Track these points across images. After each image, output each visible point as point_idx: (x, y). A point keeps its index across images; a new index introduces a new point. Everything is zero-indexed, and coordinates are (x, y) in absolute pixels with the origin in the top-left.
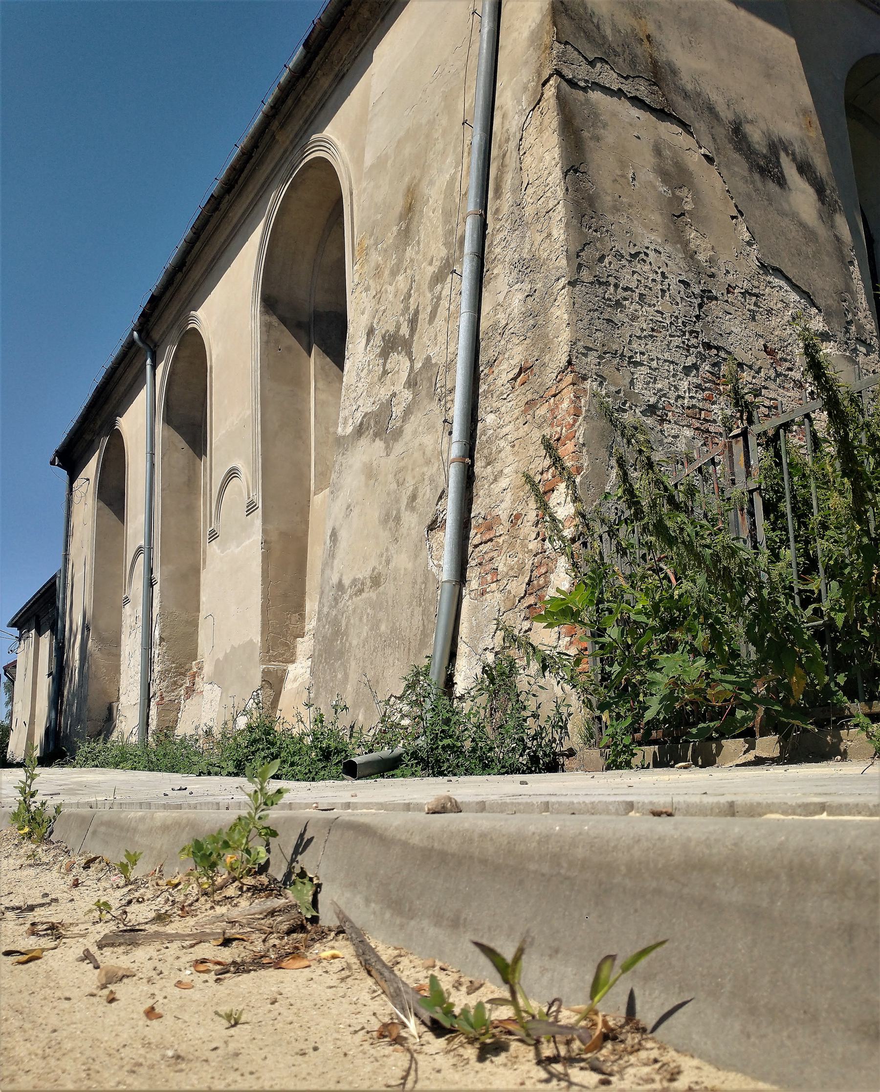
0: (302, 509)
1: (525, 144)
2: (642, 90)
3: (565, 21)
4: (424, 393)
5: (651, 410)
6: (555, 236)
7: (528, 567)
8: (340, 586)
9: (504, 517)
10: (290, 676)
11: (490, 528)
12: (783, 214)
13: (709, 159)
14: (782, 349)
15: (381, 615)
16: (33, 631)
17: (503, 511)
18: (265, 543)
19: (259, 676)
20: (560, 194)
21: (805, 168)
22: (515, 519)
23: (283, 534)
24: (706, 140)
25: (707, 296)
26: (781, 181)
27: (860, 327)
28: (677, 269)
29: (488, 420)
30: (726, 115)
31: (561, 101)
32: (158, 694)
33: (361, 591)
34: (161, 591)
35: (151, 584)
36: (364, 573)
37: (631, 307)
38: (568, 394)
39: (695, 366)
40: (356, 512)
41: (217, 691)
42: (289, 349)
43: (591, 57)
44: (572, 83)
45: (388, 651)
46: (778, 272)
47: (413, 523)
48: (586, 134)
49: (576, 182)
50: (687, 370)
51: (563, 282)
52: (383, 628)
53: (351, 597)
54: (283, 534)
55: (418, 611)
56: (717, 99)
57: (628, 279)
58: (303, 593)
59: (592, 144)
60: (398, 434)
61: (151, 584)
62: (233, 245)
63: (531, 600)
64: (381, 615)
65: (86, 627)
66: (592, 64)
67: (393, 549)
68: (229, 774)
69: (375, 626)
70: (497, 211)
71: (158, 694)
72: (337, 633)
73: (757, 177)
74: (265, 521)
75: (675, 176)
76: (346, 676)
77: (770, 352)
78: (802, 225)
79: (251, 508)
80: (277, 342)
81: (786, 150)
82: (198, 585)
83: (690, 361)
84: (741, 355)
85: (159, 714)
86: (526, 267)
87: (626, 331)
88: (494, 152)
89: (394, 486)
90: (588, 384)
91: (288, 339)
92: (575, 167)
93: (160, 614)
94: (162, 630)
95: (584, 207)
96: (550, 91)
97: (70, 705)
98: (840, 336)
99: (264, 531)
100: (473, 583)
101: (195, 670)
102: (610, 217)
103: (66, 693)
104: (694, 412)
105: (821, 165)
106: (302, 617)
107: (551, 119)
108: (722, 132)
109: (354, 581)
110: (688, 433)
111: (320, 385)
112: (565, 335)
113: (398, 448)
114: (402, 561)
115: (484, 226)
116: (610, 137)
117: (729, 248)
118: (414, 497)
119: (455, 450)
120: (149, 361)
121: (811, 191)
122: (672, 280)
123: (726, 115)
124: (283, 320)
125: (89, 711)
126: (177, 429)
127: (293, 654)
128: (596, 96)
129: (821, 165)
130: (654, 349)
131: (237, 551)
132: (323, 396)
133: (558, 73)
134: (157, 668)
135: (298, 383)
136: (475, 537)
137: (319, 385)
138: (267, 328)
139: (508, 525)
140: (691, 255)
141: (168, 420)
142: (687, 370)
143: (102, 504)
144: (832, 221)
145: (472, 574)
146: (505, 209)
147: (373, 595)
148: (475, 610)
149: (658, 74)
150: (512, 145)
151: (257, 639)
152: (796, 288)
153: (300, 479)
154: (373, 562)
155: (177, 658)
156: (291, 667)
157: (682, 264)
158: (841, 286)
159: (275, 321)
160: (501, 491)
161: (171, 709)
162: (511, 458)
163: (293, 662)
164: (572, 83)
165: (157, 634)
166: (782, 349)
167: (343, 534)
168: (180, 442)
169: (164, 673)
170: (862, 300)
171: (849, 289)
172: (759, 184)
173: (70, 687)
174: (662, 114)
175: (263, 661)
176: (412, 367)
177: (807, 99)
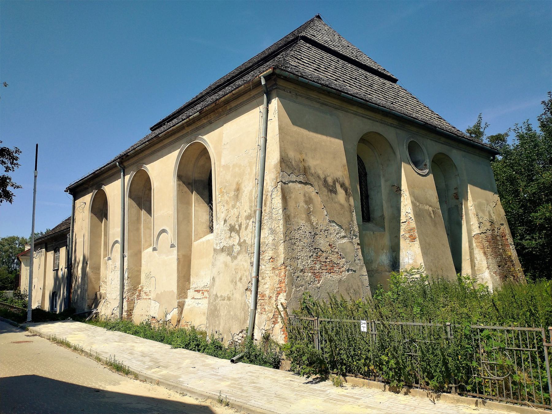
0: (189, 247)
1: (273, 196)
2: (301, 178)
3: (283, 164)
4: (244, 250)
5: (302, 270)
6: (280, 227)
7: (273, 311)
8: (216, 295)
9: (267, 295)
10: (186, 304)
11: (263, 297)
12: (335, 203)
13: (317, 193)
14: (333, 244)
15: (231, 309)
16: (44, 250)
17: (267, 293)
18: (178, 259)
19: (177, 304)
20: (282, 217)
21: (342, 185)
22: (270, 297)
23: (184, 256)
24: (317, 188)
25: (316, 234)
26: (335, 192)
27: (354, 231)
28: (308, 229)
29: (262, 267)
30: (322, 176)
31: (282, 189)
32: (127, 297)
33: (224, 300)
34: (128, 260)
35: (123, 257)
36: (225, 295)
37: (297, 243)
38: (283, 271)
39: (312, 255)
40: (221, 275)
41: (158, 304)
42: (186, 192)
43: (289, 173)
44: (285, 183)
45: (233, 320)
46: (334, 222)
47: (241, 287)
48: (288, 197)
49: (285, 213)
50: (310, 257)
51: (282, 241)
52: (232, 313)
53: (220, 300)
54: (184, 256)
55: (243, 312)
56: (320, 172)
57: (297, 236)
58: (190, 275)
59: (288, 200)
60: (235, 258)
61: (123, 257)
62: (164, 151)
63: (274, 320)
64: (231, 309)
65: (85, 262)
66: (289, 175)
67: (234, 291)
68: (183, 348)
69: (229, 312)
70: (265, 210)
71: (127, 297)
72: (216, 309)
73: (329, 193)
74: (178, 252)
75: (309, 201)
76: (220, 324)
77: (330, 245)
78: (341, 204)
79: (172, 246)
80: (182, 190)
81: (338, 182)
82: (141, 257)
83: (311, 254)
84: (323, 249)
85: (128, 305)
86: (273, 231)
87: (296, 251)
88: (264, 192)
89: (234, 272)
90: (288, 268)
91: (186, 189)
92: (285, 208)
93: (128, 269)
94: (128, 275)
95: (287, 218)
96: (279, 186)
97: (76, 291)
98: (349, 236)
99: (178, 255)
100: (259, 310)
101: (140, 288)
102: (293, 220)
103: (73, 285)
104: (311, 268)
105: (347, 183)
106: (190, 283)
107: (280, 193)
108: (321, 183)
109: (221, 296)
110: (310, 274)
111: (196, 205)
112: (282, 256)
113: (236, 262)
114: (237, 296)
115: (262, 212)
116: (293, 196)
117: (321, 219)
118: (241, 279)
119: (254, 274)
120: (122, 173)
121: (343, 192)
122: (307, 232)
123: (322, 176)
124: (184, 183)
125: (88, 295)
126: (133, 200)
127: (187, 295)
128: (290, 184)
129: (347, 183)
130: (303, 254)
131: (166, 258)
132: (197, 208)
133: (282, 181)
134: (126, 288)
135: (189, 204)
136: (259, 297)
137: (196, 205)
138: (179, 186)
139: (268, 298)
140: (312, 224)
141: (130, 196)
142: (310, 257)
143: (92, 214)
144: (349, 199)
145: (258, 307)
146: (267, 211)
147: (228, 302)
148: (259, 318)
149: (305, 171)
150: (269, 194)
151: (176, 291)
152: (338, 225)
153: (189, 236)
154: (228, 293)
155: (131, 285)
156: (186, 300)
157: (310, 227)
158: (350, 220)
159: (181, 183)
160: (266, 287)
161: (132, 303)
162: (269, 281)
163: (187, 298)
164: (285, 183)
165: (126, 275)
166: (333, 244)
167: (217, 279)
168: (135, 205)
169: (129, 290)
170: (355, 222)
171: (352, 221)
172: (330, 195)
173: (76, 283)
174: (306, 184)
175: (177, 299)
176: (240, 240)
177: (345, 161)
